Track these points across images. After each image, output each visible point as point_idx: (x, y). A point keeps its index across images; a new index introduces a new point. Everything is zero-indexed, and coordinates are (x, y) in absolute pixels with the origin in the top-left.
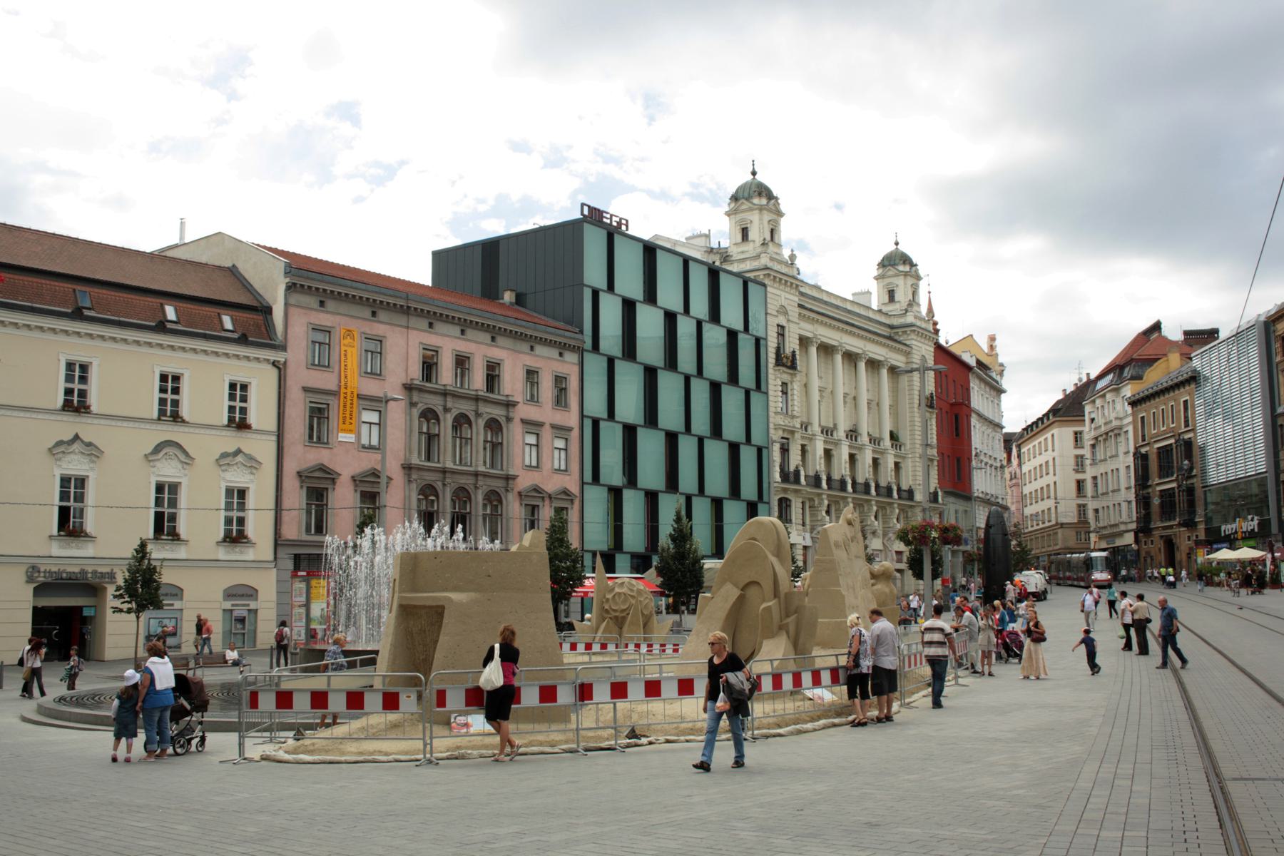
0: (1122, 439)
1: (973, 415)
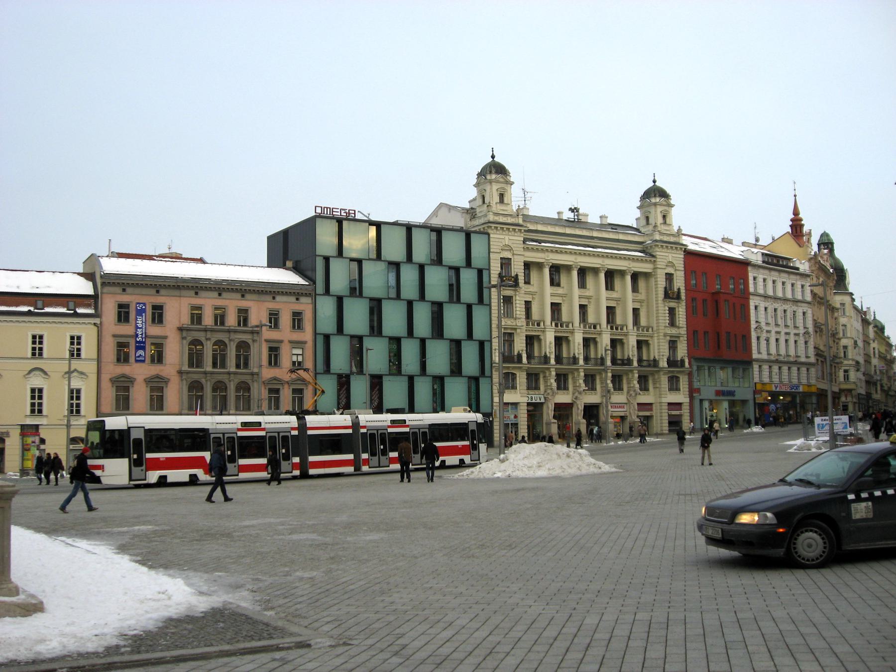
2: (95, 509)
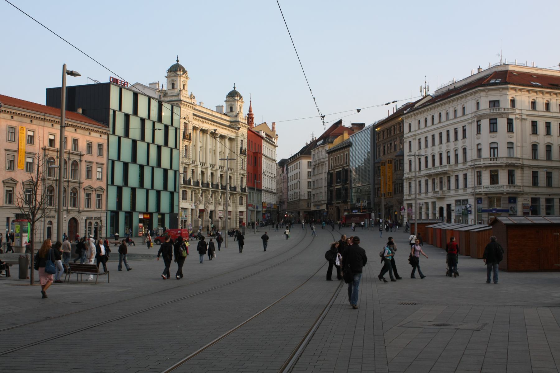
0: (324, 166)
1: (263, 156)
2: (400, 278)
